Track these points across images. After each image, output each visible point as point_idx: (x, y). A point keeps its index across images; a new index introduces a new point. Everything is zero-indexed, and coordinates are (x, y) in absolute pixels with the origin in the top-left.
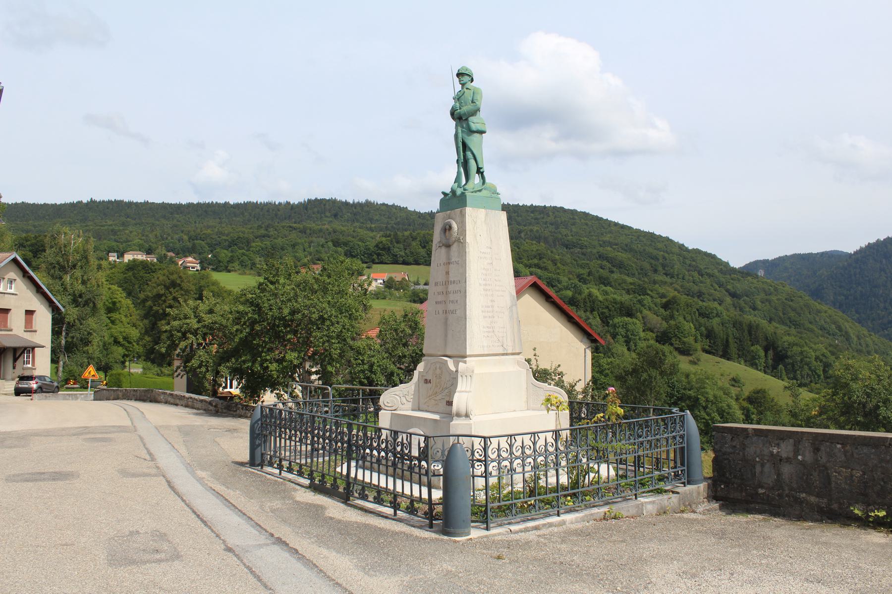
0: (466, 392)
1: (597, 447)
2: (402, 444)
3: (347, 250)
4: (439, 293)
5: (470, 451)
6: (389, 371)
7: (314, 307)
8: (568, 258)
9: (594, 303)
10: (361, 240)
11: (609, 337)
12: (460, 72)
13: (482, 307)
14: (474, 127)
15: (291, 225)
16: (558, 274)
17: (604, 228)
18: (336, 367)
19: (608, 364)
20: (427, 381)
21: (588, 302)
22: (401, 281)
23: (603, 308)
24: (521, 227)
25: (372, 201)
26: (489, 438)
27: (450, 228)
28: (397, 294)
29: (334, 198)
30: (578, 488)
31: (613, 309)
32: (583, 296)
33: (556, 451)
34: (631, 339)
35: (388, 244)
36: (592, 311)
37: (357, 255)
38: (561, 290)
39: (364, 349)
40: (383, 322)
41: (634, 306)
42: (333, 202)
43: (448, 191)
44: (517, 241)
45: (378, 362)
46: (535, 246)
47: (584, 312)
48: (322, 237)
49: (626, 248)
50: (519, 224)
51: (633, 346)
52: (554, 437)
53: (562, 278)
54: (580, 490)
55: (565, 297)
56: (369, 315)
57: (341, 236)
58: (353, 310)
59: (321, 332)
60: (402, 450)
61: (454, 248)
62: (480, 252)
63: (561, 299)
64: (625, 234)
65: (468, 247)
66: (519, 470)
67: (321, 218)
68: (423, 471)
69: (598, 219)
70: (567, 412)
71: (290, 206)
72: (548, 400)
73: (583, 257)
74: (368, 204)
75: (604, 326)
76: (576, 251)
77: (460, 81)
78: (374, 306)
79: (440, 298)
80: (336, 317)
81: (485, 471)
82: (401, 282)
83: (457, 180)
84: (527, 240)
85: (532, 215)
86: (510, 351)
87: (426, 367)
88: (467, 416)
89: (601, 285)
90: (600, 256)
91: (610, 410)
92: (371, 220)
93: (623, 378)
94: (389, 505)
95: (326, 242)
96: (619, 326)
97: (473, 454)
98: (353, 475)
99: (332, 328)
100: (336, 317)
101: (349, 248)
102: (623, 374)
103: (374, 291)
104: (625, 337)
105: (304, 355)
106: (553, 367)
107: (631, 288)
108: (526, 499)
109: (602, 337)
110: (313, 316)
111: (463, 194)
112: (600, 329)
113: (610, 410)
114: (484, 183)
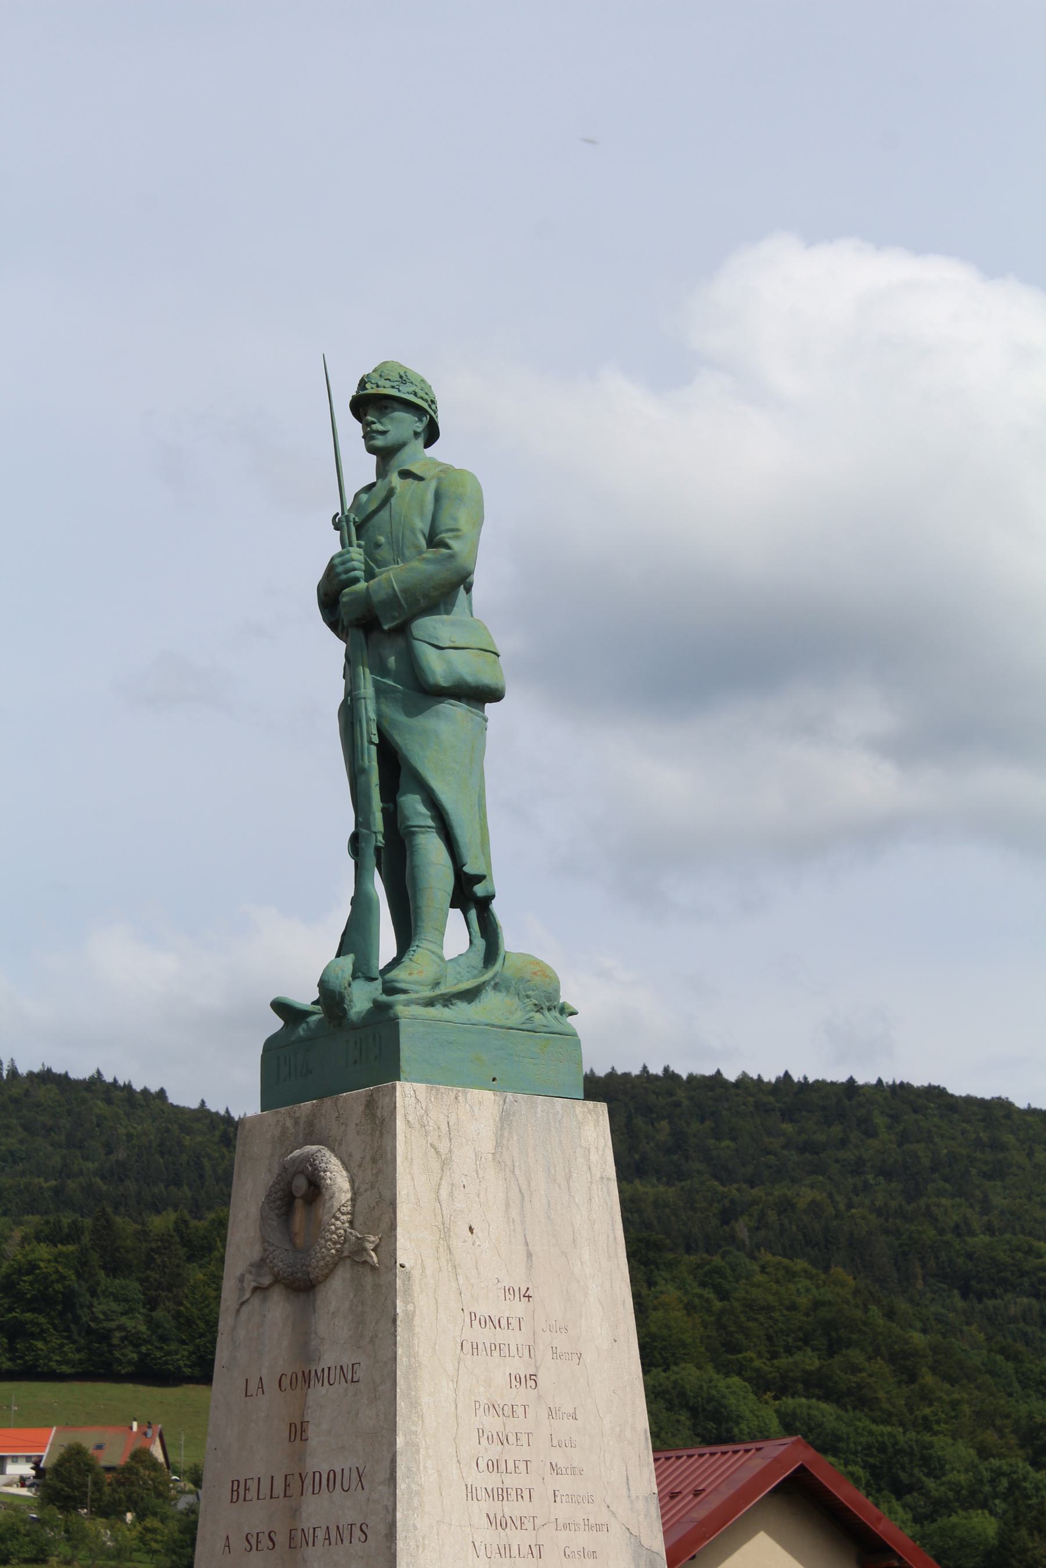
12: (371, 389)
16: (926, 1425)
22: (128, 1469)
35: (62, 1278)
38: (940, 1507)
44: (717, 1260)
46: (804, 1283)
53: (943, 1446)
62: (473, 1315)
65: (408, 1291)
76: (1012, 1310)
77: (368, 436)
82: (126, 1475)
85: (787, 1127)
114: (492, 952)
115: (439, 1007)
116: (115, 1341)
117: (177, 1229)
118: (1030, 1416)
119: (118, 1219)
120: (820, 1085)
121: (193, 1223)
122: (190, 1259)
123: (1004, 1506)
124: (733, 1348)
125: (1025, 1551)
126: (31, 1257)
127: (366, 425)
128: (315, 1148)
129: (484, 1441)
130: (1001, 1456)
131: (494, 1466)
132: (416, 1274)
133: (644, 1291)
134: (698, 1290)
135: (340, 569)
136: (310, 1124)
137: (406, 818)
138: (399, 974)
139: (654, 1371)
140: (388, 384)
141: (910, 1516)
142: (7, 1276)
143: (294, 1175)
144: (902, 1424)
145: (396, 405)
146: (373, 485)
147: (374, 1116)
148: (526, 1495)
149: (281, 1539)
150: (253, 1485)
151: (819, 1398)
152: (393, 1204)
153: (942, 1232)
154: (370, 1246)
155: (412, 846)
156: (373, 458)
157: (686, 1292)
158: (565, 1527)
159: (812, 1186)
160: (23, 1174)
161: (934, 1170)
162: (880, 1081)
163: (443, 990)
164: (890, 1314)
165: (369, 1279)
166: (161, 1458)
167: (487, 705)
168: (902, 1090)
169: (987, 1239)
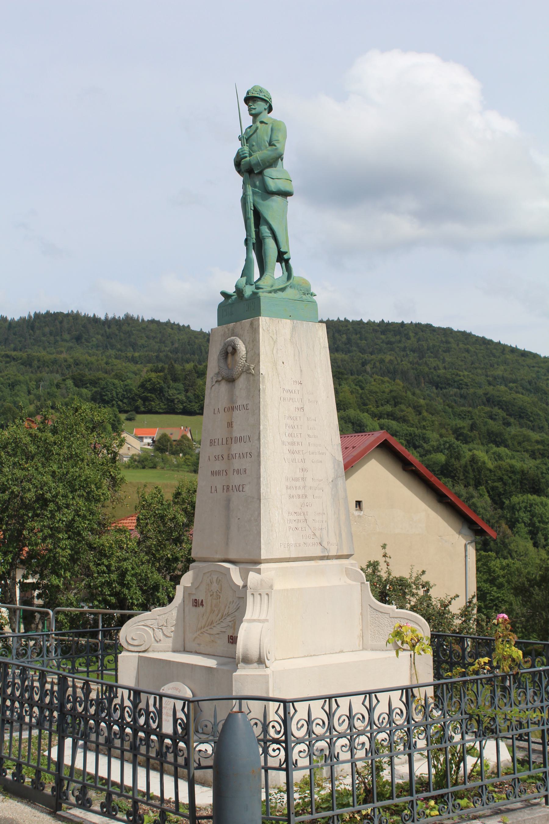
0: (259, 621)
1: (478, 715)
2: (148, 713)
3: (96, 392)
4: (216, 458)
5: (260, 726)
6: (151, 582)
7: (29, 481)
8: (439, 404)
9: (479, 472)
10: (119, 377)
11: (504, 526)
12: (250, 95)
13: (287, 479)
14: (272, 185)
15: (9, 353)
16: (424, 427)
17: (494, 356)
18: (65, 578)
19: (503, 568)
20: (197, 603)
21: (470, 471)
22: (180, 441)
23: (494, 481)
24: (366, 356)
25: (135, 316)
26: (293, 702)
27: (235, 350)
28: (174, 461)
29: (75, 312)
30: (447, 787)
31: (510, 481)
32: (463, 461)
33: (408, 723)
34: (538, 527)
35: (159, 383)
36: (477, 484)
37: (112, 401)
38: (428, 452)
39: (111, 547)
40: (145, 505)
41: (543, 478)
42: (74, 317)
43: (231, 290)
45: (133, 569)
47: (465, 486)
48: (57, 372)
49: (529, 387)
50: (363, 351)
51: (543, 540)
52: (404, 699)
53: (429, 434)
54: (451, 789)
55: (435, 463)
56: (120, 494)
57: (87, 370)
58: (93, 486)
59: (40, 521)
60: (147, 722)
61: (241, 382)
63: (428, 466)
64: (528, 366)
66: (345, 756)
67: (56, 341)
68: (181, 760)
69: (485, 342)
70: (430, 652)
71: (7, 324)
72: (398, 634)
73: (462, 401)
74: (129, 320)
75: (495, 509)
76: (451, 393)
77: (250, 110)
78: (128, 479)
79: (218, 466)
80: (65, 496)
81: (286, 760)
83: (246, 272)
84: (376, 376)
86: (333, 553)
87: (195, 578)
88: (261, 661)
89: (491, 445)
90: (488, 400)
91: (500, 651)
92: (134, 346)
93: (527, 590)
94: (125, 818)
95: (64, 380)
96: (520, 508)
97: (265, 730)
98: (67, 761)
99: (58, 516)
100: (65, 496)
101: (99, 389)
102: (527, 584)
103: (139, 455)
104: (529, 525)
105: (13, 559)
106: (414, 575)
107: (538, 449)
108: (357, 808)
109: (492, 527)
110: (28, 495)
111: (255, 296)
112: (490, 513)
113: (500, 651)
114: (289, 277)
115: (273, 293)
116: (176, 402)
117: (194, 368)
118: (456, 425)
119: (176, 365)
120: (393, 324)
121: (199, 366)
122: (198, 377)
123: (447, 452)
124: (365, 404)
125: (453, 465)
126: (149, 377)
127: (249, 106)
128: (234, 337)
129: (287, 427)
130: (447, 437)
131: (290, 435)
132: (266, 376)
133: (338, 387)
134: (354, 387)
135: (241, 153)
136: (233, 330)
137: (262, 234)
138: (260, 283)
139: (341, 411)
140: (256, 93)
141: (419, 455)
142: (142, 383)
143: (228, 346)
144: (417, 427)
145: (258, 100)
146: (251, 126)
147: (253, 327)
148: (300, 444)
149: (225, 457)
150: (216, 441)
151: (391, 420)
152: (259, 355)
153: (430, 369)
154: (252, 368)
155: (264, 242)
156: (252, 117)
157: (351, 387)
158: (312, 453)
159: (390, 355)
160: (146, 351)
161: (428, 349)
162: (412, 322)
163: (274, 288)
164: (414, 394)
165: (251, 378)
166: (190, 438)
167: (288, 197)
168: (418, 325)
169: (444, 371)
